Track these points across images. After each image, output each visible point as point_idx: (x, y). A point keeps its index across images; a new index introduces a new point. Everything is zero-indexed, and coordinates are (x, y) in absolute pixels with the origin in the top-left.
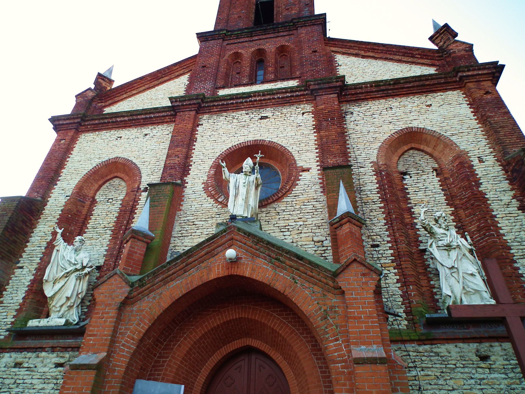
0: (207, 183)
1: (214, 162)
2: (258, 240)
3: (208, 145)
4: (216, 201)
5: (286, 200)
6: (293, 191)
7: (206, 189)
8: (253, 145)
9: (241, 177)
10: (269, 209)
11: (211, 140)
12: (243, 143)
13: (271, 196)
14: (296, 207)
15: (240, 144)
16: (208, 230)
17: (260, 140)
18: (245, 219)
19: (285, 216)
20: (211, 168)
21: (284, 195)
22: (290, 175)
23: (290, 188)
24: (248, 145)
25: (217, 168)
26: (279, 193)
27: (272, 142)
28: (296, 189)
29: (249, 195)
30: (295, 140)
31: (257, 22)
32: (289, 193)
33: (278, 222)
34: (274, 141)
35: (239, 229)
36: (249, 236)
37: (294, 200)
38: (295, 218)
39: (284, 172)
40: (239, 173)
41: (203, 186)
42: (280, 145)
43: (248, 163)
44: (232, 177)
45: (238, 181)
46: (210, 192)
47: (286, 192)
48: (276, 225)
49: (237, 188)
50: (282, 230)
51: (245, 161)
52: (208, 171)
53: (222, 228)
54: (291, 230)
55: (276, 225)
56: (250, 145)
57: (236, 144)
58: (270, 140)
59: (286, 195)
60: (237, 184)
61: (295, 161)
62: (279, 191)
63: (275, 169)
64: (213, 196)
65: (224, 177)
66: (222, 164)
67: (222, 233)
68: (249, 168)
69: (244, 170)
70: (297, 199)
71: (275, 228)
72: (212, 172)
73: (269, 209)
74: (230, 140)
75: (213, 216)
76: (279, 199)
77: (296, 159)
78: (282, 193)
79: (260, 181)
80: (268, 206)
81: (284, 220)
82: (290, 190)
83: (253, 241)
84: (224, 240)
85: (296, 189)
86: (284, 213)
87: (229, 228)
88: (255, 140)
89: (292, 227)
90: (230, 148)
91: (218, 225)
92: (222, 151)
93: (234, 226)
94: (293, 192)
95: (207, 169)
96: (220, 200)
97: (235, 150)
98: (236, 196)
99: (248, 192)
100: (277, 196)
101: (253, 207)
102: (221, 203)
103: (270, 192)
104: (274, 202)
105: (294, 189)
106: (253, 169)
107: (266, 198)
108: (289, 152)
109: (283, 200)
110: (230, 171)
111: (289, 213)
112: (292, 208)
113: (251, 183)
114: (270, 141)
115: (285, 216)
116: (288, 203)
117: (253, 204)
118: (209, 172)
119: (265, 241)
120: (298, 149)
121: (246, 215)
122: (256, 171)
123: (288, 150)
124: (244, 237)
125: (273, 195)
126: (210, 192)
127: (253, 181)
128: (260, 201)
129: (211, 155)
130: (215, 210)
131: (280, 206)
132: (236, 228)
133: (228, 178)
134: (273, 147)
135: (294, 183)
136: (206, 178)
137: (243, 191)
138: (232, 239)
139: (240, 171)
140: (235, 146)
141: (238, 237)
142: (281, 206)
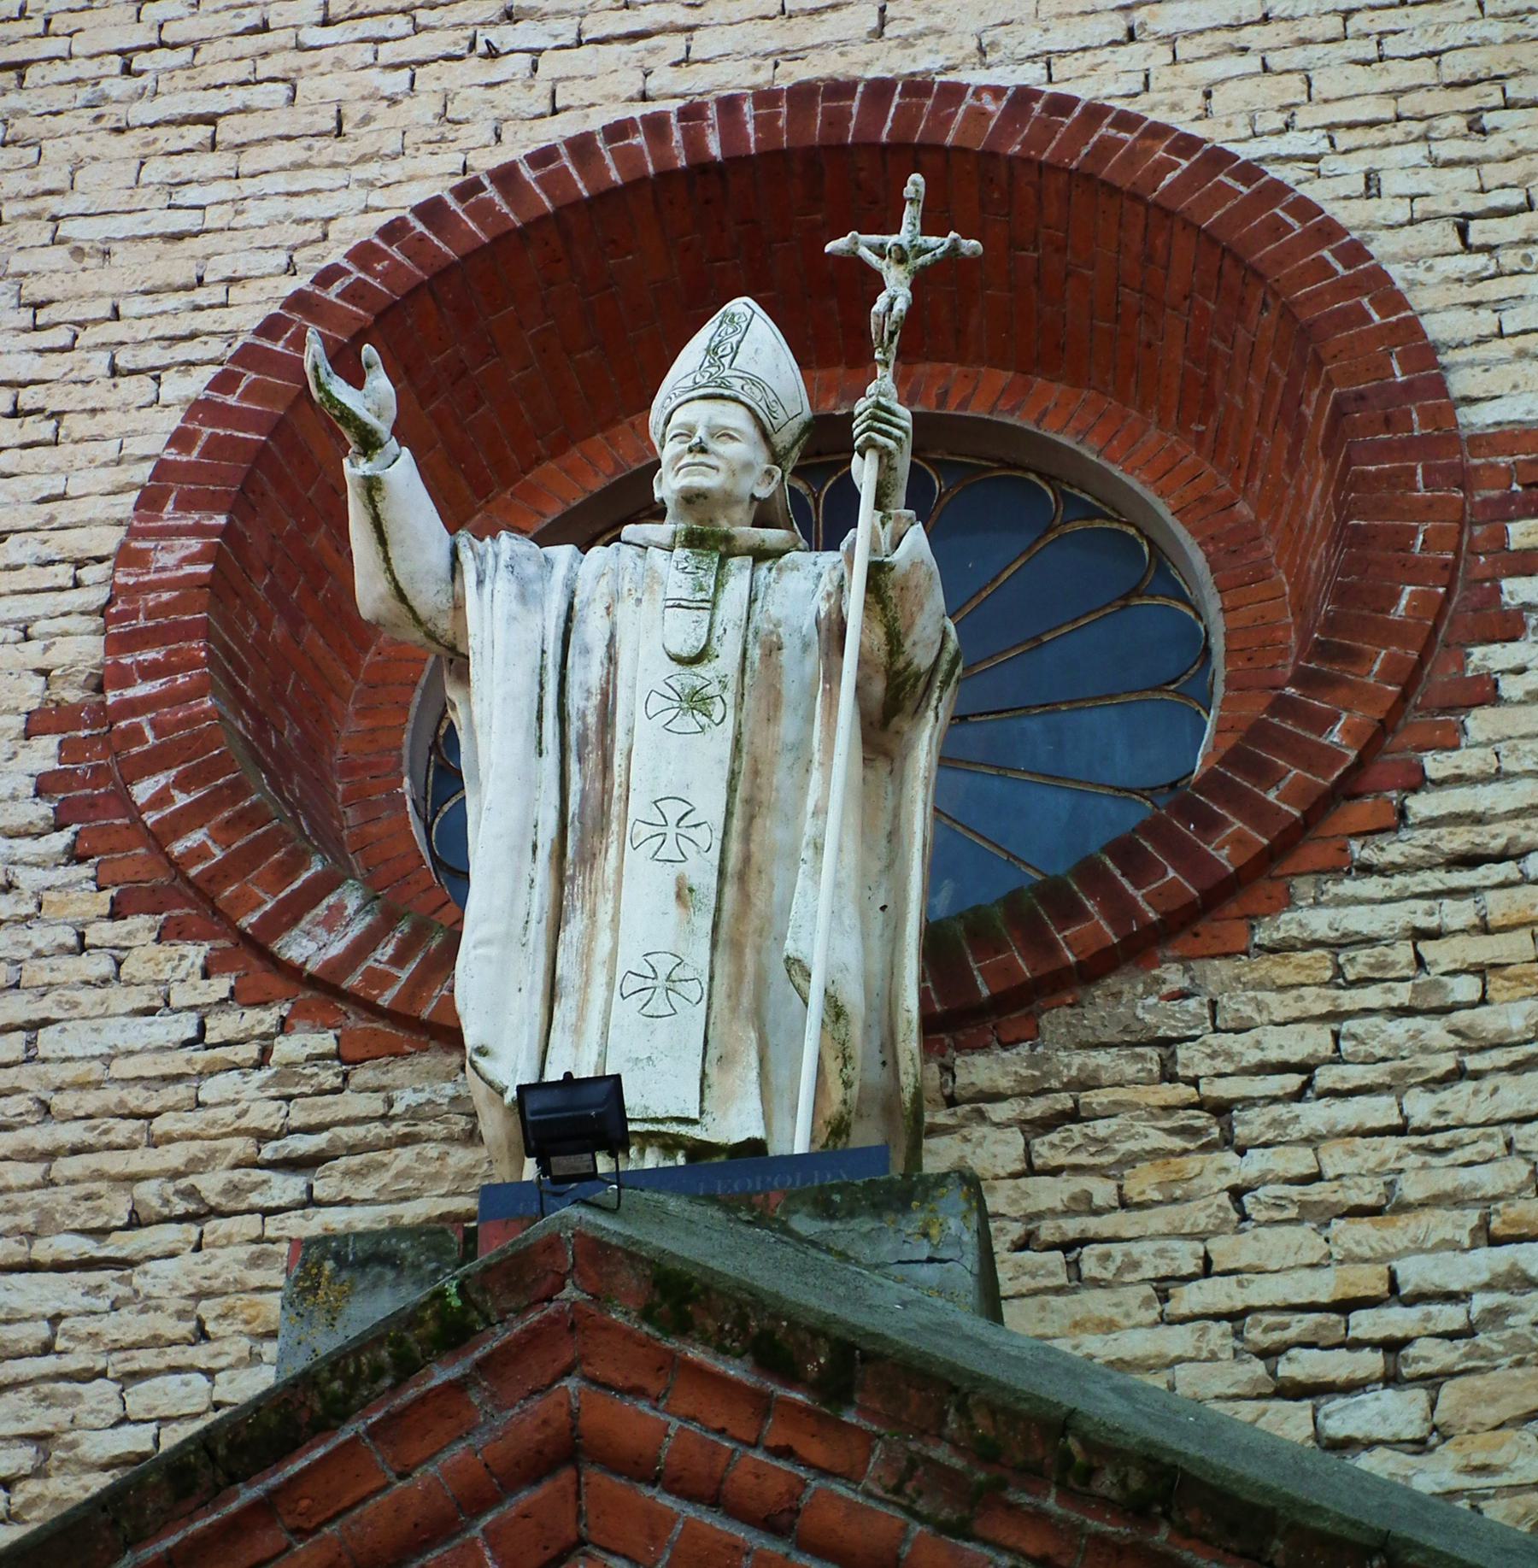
0: (103, 715)
1: (198, 409)
2: (986, 1453)
3: (104, 183)
4: (254, 963)
5: (1319, 922)
6: (1419, 782)
7: (84, 803)
8: (772, 157)
9: (639, 594)
10: (1074, 1062)
11: (143, 112)
12: (618, 131)
13: (1090, 873)
14: (1488, 1021)
15: (581, 146)
16: (140, 1398)
17: (880, 90)
18: (731, 1174)
19: (1335, 1159)
20: (150, 500)
21: (1299, 846)
22: (1367, 563)
23: (1374, 743)
24: (702, 168)
25: (261, 479)
26: (1210, 824)
27: (1062, 104)
28: (1468, 760)
29: (771, 831)
30: (1400, 74)
31: (123, 73)
32: (1360, 812)
33: (1224, 1249)
34: (1084, 91)
35: (678, 1296)
36: (836, 1387)
37: (1457, 914)
38: (1489, 1179)
39: (1248, 536)
40: (607, 533)
41: (44, 754)
42: (1187, 144)
43: (730, 378)
44: (503, 586)
45: (592, 629)
46: (158, 838)
47: (1321, 806)
48: (1190, 1298)
49: (581, 740)
50: (1302, 1366)
51: (690, 359)
52: (109, 540)
53: (373, 1306)
54: (1433, 1355)
55: (1190, 1298)
56: (735, 162)
57: (514, 150)
58: (1031, 75)
59: (1313, 853)
60: (586, 674)
61: (1424, 353)
62: (1187, 805)
63: (1117, 503)
64: (203, 893)
65: (369, 593)
66: (342, 391)
67: (407, 1368)
68: (744, 449)
69: (667, 487)
70: (1498, 906)
71: (1178, 1340)
72: (176, 558)
73: (1074, 1062)
74: (422, 109)
75: (211, 1184)
76: (1218, 913)
77: (1436, 327)
78: (1258, 813)
79: (930, 627)
80: (1055, 1021)
81: (1323, 1215)
82: (1374, 780)
83: (909, 1477)
84: (446, 1463)
85: (1468, 760)
86: (1314, 1115)
87: (524, 1275)
88: (803, 94)
89: (1451, 1316)
90: (431, 211)
91: (324, 1266)
92: (311, 263)
93: (595, 1251)
94: (1421, 805)
95: (100, 517)
96: (304, 947)
97: (507, 241)
98: (575, 847)
99: (747, 795)
100: (1191, 860)
101: (853, 997)
102: (321, 992)
103: (1050, 830)
104: (1137, 948)
105: (1435, 764)
106: (820, 452)
107: (1012, 900)
108: (1330, 231)
109: (1286, 925)
110: (466, 502)
111: (1380, 1110)
112: (1435, 1030)
113: (799, 667)
114: (1024, 96)
115: (1335, 1159)
116: (1360, 962)
117: (849, 951)
118: (126, 557)
119: (1107, 1450)
120: (1454, 190)
121: (735, 1122)
122: (864, 472)
123: (1305, 208)
124: (763, 1405)
125: (1126, 852)
126: (158, 838)
127: (834, 632)
128: (938, 946)
129: (144, 321)
130: (246, 1097)
131: (1236, 1005)
132: (628, 1279)
133: (429, 597)
134: (1086, 178)
135: (1438, 676)
136: (82, 649)
137: (672, 766)
138: (566, 1451)
139: (614, 507)
140: (506, 176)
141: (659, 1424)
142: (1252, 1012)
